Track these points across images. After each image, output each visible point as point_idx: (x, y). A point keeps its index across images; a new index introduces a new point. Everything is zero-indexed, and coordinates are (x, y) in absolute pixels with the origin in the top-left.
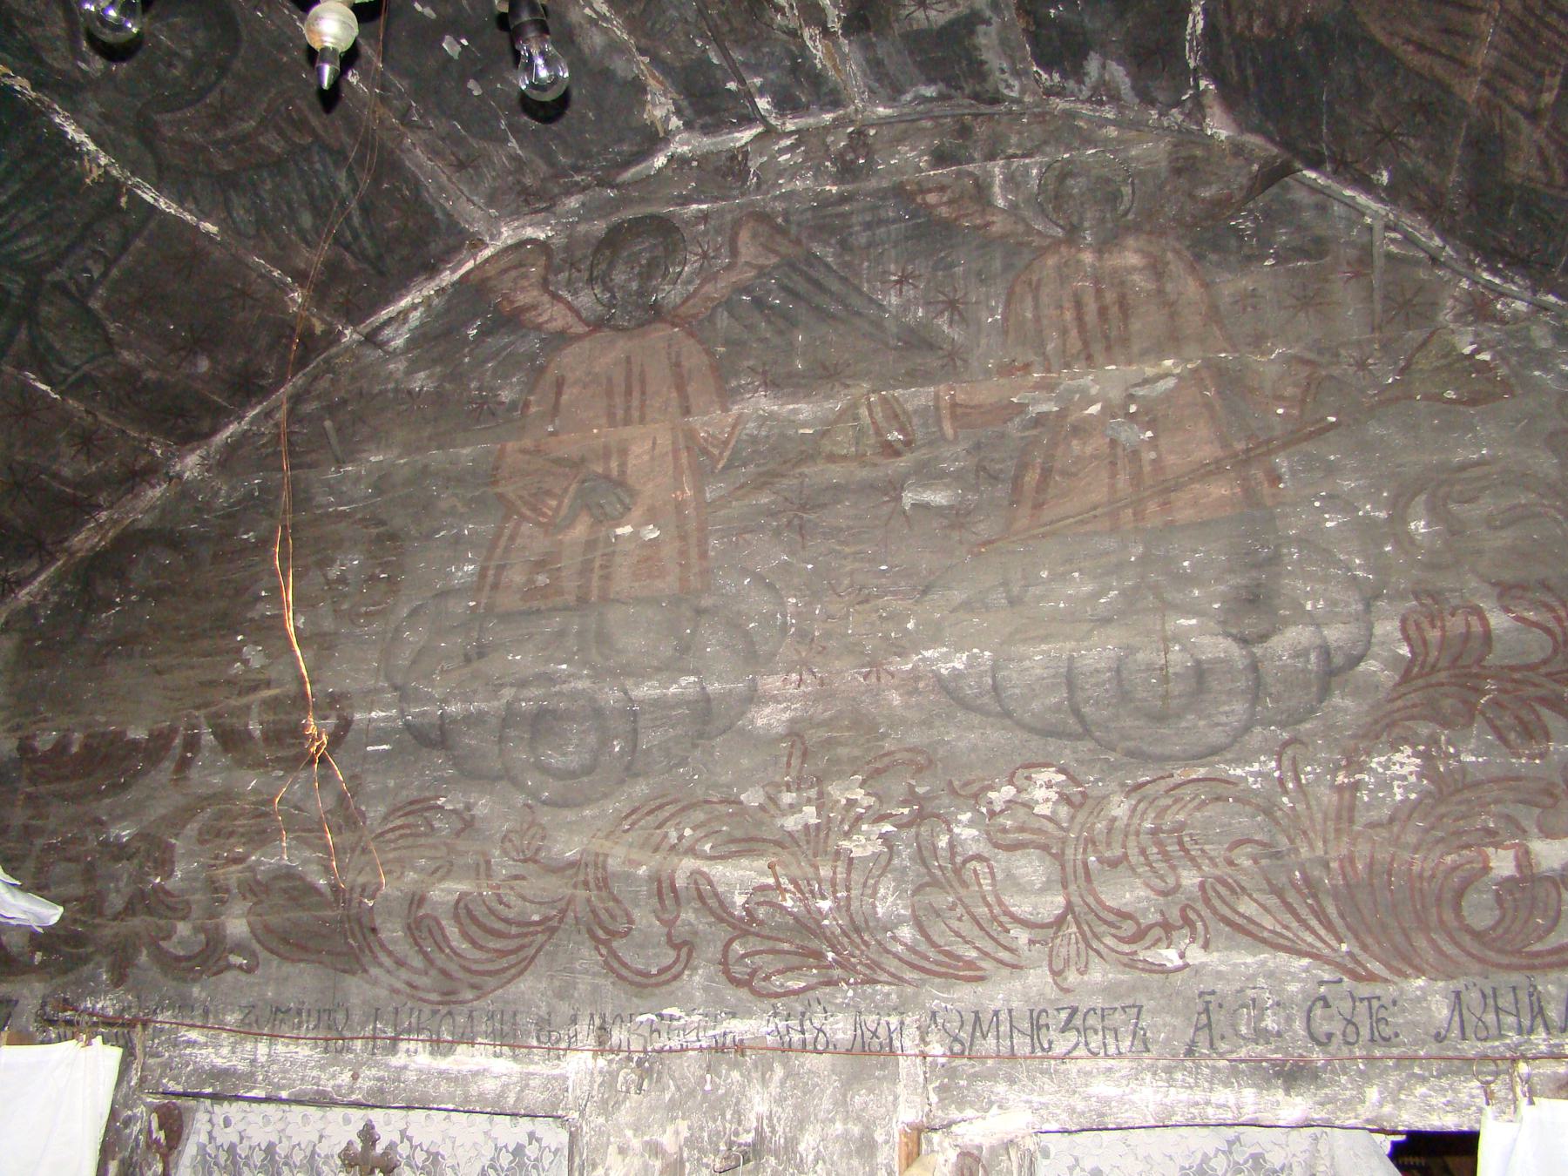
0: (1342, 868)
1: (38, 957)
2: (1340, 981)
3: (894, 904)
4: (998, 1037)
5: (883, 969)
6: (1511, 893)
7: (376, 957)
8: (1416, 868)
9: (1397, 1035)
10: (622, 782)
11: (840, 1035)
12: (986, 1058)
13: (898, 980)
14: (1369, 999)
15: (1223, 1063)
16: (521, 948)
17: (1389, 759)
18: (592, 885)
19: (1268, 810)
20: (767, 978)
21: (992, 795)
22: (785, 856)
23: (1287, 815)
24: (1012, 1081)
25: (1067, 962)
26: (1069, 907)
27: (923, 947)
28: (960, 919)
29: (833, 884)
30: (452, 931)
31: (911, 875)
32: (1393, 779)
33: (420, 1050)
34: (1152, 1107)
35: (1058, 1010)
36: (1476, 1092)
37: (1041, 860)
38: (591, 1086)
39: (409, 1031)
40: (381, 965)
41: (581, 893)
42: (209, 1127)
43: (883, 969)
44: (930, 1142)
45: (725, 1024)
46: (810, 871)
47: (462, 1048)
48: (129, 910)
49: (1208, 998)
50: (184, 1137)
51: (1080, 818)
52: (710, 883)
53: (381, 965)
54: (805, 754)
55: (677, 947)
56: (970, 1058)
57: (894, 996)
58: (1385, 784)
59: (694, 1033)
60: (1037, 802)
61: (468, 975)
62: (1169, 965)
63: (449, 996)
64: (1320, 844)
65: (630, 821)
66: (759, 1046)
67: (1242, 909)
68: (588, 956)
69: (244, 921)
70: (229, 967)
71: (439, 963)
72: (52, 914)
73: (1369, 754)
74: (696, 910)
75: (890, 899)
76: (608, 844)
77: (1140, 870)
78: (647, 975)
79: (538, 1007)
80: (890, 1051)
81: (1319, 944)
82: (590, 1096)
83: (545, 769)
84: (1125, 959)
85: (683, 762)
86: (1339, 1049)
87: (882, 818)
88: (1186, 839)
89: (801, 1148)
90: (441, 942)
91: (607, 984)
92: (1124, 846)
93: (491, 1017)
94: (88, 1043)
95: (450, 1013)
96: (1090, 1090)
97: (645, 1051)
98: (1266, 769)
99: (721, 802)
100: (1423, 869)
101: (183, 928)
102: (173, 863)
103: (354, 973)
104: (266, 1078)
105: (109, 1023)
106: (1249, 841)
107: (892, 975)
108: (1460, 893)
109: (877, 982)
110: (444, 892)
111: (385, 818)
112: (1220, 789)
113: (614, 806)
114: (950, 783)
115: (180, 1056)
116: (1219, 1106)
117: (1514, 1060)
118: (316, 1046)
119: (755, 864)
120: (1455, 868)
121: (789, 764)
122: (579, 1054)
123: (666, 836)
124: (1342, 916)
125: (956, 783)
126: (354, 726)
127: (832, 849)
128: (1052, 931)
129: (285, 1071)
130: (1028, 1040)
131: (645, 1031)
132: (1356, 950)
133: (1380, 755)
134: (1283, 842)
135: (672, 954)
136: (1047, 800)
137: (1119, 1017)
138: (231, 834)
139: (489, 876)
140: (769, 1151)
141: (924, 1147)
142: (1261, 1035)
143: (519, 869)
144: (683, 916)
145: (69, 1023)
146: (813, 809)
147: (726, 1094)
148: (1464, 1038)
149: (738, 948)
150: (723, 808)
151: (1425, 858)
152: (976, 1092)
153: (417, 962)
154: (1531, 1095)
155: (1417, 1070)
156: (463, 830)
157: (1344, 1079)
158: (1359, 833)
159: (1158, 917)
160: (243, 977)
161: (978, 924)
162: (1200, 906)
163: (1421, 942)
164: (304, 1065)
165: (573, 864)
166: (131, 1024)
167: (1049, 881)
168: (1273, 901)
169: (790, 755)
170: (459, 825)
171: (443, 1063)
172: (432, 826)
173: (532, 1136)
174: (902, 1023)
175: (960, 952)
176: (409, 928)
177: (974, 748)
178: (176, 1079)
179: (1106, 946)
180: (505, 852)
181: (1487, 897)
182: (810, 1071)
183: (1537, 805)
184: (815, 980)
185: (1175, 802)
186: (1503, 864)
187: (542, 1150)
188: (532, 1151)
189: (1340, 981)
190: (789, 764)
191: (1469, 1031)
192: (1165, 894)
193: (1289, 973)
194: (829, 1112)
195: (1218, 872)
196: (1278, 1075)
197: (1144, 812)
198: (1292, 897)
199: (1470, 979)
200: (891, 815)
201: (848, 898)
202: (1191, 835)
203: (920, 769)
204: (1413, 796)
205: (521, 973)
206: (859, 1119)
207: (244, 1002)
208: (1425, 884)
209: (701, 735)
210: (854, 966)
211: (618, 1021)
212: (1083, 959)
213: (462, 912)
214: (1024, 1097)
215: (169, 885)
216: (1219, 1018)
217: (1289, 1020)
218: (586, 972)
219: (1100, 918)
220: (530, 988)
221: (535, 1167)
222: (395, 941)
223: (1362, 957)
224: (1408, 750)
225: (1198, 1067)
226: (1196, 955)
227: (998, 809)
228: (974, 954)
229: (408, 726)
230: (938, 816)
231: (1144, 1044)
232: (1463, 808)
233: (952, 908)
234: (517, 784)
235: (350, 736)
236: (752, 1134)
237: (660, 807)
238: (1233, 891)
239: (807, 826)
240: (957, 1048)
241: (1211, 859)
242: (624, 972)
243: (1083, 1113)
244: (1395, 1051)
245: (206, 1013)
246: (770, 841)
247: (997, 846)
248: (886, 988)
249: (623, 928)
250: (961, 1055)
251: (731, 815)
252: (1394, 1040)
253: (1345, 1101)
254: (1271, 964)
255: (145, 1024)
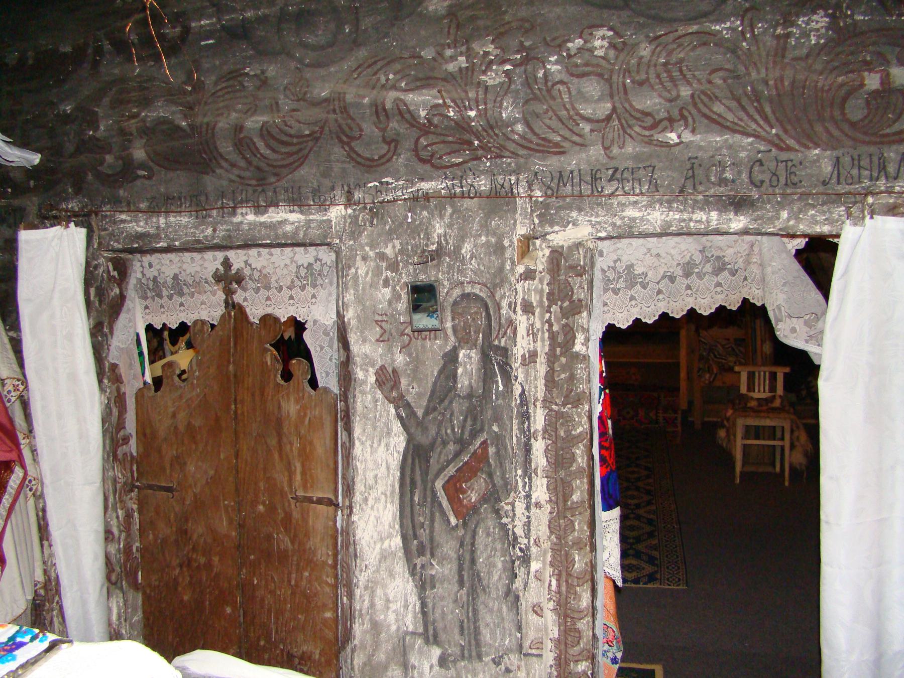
0: (776, 84)
1: (32, 183)
2: (770, 150)
3: (512, 111)
4: (572, 186)
5: (507, 150)
6: (875, 99)
7: (219, 164)
8: (820, 85)
9: (801, 182)
10: (352, 50)
11: (483, 188)
12: (565, 197)
13: (515, 155)
14: (786, 161)
15: (700, 197)
16: (301, 150)
17: (810, 19)
18: (337, 111)
19: (734, 50)
20: (441, 157)
21: (570, 45)
22: (449, 87)
23: (745, 54)
24: (580, 210)
25: (612, 141)
26: (614, 110)
27: (530, 135)
28: (550, 119)
29: (477, 102)
30: (261, 145)
31: (522, 95)
32: (811, 31)
33: (249, 212)
34: (659, 223)
35: (607, 169)
36: (842, 213)
37: (599, 83)
38: (345, 225)
39: (241, 202)
40: (222, 167)
41: (332, 116)
42: (141, 269)
43: (507, 150)
44: (534, 245)
45: (417, 185)
46: (463, 95)
47: (271, 209)
48: (78, 151)
49: (693, 161)
50: (128, 274)
51: (622, 57)
52: (406, 105)
53: (222, 167)
54: (458, 27)
55: (389, 144)
56: (557, 198)
57: (513, 165)
58: (806, 34)
59: (400, 191)
60: (596, 48)
61: (271, 168)
62: (672, 142)
63: (262, 181)
64: (763, 71)
65: (357, 72)
66: (437, 195)
67: (715, 109)
68: (338, 152)
69: (143, 151)
70: (139, 177)
71: (255, 163)
72: (36, 158)
73: (798, 16)
74: (398, 121)
75: (510, 109)
76: (345, 86)
77: (657, 87)
78: (372, 160)
79: (312, 183)
80: (511, 196)
81: (759, 130)
82: (345, 230)
83: (306, 46)
84: (646, 139)
85: (386, 35)
86: (767, 189)
87: (504, 62)
88: (684, 68)
89: (463, 251)
90: (255, 151)
91: (349, 166)
92: (647, 73)
93: (286, 191)
94: (67, 227)
95: (263, 191)
96: (624, 214)
97: (374, 203)
98: (733, 26)
99: (410, 58)
100: (824, 85)
101: (109, 158)
102: (97, 121)
103: (208, 174)
104: (166, 236)
105: (76, 215)
106: (721, 69)
107: (513, 153)
108: (845, 100)
109: (504, 157)
110: (254, 123)
111: (216, 84)
112: (705, 38)
113: (347, 65)
114: (545, 39)
115: (118, 229)
116: (697, 222)
117: (866, 195)
118: (191, 216)
119: (431, 92)
120: (842, 85)
121: (449, 32)
122: (337, 207)
123: (379, 79)
124: (774, 112)
125: (548, 39)
126: (192, 31)
127: (475, 81)
128: (604, 124)
129: (176, 231)
130: (590, 187)
131: (373, 192)
132: (781, 133)
133: (804, 16)
134: (742, 69)
135: (386, 147)
136: (602, 47)
137: (642, 172)
138: (129, 102)
139: (278, 111)
140: (445, 253)
141: (531, 248)
142: (723, 182)
143: (295, 105)
144: (391, 125)
145: (55, 217)
146: (464, 58)
147: (420, 224)
148: (839, 183)
149: (423, 141)
150: (411, 61)
151: (826, 79)
152: (560, 216)
153: (242, 164)
154: (872, 214)
155: (810, 201)
156: (261, 86)
157: (768, 206)
158: (788, 63)
159: (666, 115)
160: (146, 182)
161: (561, 120)
162: (691, 108)
163: (819, 128)
164: (186, 227)
165: (326, 100)
166: (88, 215)
167: (602, 95)
168: (733, 104)
169: (449, 28)
170: (258, 83)
171: (263, 219)
172: (244, 87)
173: (317, 259)
174: (518, 179)
175: (551, 138)
176: (236, 145)
177: (559, 17)
178: (118, 241)
179: (635, 132)
180: (286, 96)
181: (861, 102)
182: (466, 209)
183: (898, 46)
184: (467, 158)
185: (679, 46)
186: (872, 82)
187: (323, 265)
188: (317, 266)
189: (770, 150)
190: (449, 32)
191: (842, 180)
192: (670, 101)
193: (740, 146)
194: (477, 231)
195: (703, 88)
196: (731, 204)
197: (660, 53)
198: (745, 101)
199: (846, 150)
200: (510, 60)
201: (486, 109)
202: (687, 66)
203: (527, 31)
204: (822, 41)
205: (302, 164)
206: (494, 234)
207: (149, 196)
208: (825, 95)
209: (396, 18)
210: (490, 148)
211: (358, 187)
212: (622, 140)
213: (265, 133)
214: (587, 218)
215: (99, 135)
216: (699, 172)
217: (740, 173)
218: (338, 161)
219: (632, 116)
220: (307, 173)
221: (319, 275)
222: (229, 153)
223: (784, 137)
224: (821, 13)
225: (686, 200)
226: (687, 136)
227: (572, 53)
228: (559, 139)
229: (223, 27)
230: (538, 59)
231: (655, 187)
232: (852, 48)
233: (546, 112)
234: (290, 56)
235: (190, 38)
236: (436, 245)
237: (375, 63)
238: (710, 98)
239: (460, 69)
240: (549, 192)
241: (698, 80)
242: (359, 159)
243: (620, 226)
244: (799, 191)
245: (129, 204)
246: (439, 79)
247: (572, 75)
248: (509, 160)
249: (357, 134)
250: (552, 196)
251: (416, 65)
252: (799, 184)
253: (769, 219)
254: (730, 141)
255: (96, 215)
